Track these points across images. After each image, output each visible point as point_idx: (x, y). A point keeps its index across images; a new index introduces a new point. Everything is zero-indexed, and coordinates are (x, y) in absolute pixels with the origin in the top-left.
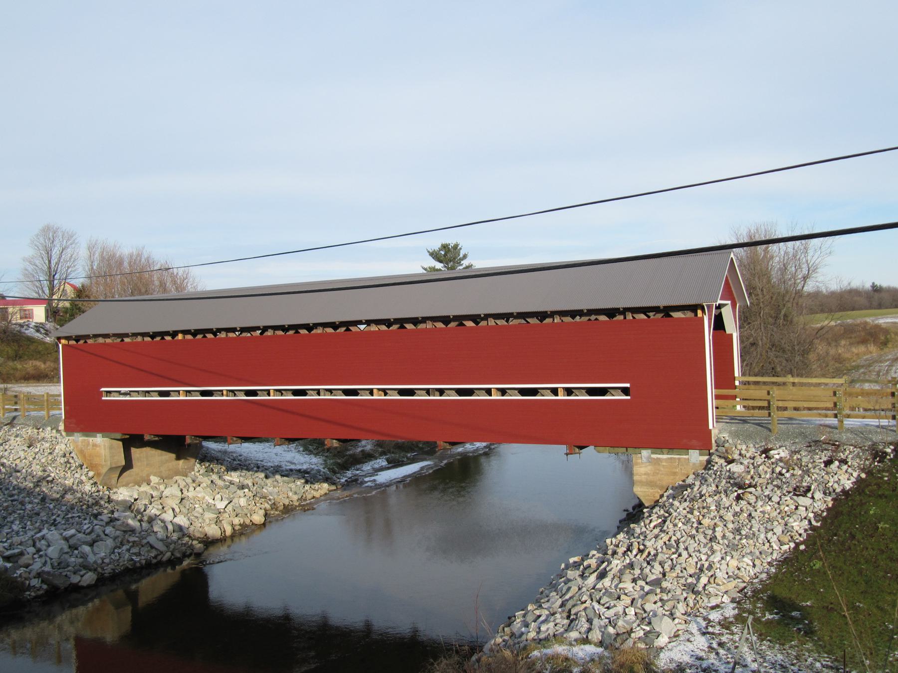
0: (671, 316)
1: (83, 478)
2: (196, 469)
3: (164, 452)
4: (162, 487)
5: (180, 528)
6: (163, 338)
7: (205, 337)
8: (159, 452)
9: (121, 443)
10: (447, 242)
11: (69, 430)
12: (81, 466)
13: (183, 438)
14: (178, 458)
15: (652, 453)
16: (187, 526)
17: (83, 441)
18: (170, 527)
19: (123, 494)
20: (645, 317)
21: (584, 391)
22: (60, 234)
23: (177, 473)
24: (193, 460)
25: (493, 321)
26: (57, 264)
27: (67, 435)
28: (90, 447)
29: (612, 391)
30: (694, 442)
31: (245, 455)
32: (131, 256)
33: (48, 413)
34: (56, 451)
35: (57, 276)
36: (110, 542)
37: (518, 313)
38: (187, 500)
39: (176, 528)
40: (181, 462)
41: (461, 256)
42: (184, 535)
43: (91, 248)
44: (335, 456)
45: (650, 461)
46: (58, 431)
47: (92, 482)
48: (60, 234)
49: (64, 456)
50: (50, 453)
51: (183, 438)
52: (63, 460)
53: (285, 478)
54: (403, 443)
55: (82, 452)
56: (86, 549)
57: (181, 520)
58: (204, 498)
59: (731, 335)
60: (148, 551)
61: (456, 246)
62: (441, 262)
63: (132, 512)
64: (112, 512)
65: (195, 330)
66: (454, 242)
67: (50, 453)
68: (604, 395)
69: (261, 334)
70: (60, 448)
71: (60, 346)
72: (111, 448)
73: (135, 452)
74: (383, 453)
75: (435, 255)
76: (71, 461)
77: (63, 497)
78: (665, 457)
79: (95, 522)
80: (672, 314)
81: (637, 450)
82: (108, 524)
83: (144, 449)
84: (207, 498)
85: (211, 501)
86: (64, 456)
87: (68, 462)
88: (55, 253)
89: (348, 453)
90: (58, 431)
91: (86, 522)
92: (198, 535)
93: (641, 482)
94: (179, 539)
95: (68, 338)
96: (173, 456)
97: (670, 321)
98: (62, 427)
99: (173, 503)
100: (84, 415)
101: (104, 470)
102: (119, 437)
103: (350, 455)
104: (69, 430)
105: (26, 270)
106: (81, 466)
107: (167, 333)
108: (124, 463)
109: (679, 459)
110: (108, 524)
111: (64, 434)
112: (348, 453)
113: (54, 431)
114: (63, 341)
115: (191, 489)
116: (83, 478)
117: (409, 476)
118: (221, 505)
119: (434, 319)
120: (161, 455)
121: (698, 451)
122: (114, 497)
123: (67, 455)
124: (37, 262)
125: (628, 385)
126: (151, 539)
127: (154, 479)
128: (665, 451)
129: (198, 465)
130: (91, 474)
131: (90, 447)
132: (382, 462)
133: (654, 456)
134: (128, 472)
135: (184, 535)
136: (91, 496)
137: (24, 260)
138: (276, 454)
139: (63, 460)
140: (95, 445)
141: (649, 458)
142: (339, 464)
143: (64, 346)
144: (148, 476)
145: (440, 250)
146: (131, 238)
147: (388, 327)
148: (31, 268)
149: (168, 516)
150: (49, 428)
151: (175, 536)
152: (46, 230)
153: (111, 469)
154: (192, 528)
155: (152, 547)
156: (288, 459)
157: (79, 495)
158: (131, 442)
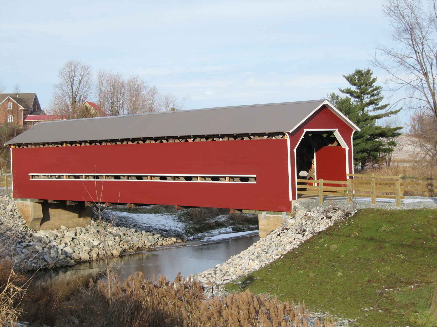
0: (188, 141)
1: (20, 224)
2: (91, 224)
3: (70, 213)
4: (65, 232)
5: (66, 253)
6: (243, 139)
7: (213, 140)
8: (67, 212)
9: (40, 205)
10: (360, 69)
11: (15, 197)
12: (20, 217)
13: (65, 202)
14: (80, 217)
15: (267, 213)
16: (71, 252)
17: (21, 203)
18: (60, 252)
19: (41, 234)
20: (179, 142)
21: (239, 179)
22: (79, 67)
23: (79, 225)
24: (89, 219)
25: (149, 141)
26: (78, 89)
27: (15, 200)
28: (24, 207)
29: (250, 179)
30: (284, 208)
31: (136, 219)
32: (129, 82)
33: (7, 188)
34: (7, 208)
35: (77, 98)
36: (22, 256)
37: (110, 140)
38: (75, 238)
39: (63, 253)
40: (81, 219)
41: (371, 80)
42: (67, 257)
43: (100, 78)
44: (195, 223)
45: (266, 217)
46: (10, 197)
47: (24, 226)
48: (79, 67)
49: (12, 211)
50: (4, 209)
51: (65, 202)
52: (10, 213)
53: (148, 233)
54: (252, 218)
55: (21, 209)
56: (8, 258)
57: (68, 249)
58: (88, 239)
59: (345, 149)
60: (42, 263)
61: (368, 73)
62: (355, 85)
63: (41, 243)
64: (30, 242)
65: (207, 135)
66: (366, 69)
67: (4, 209)
68: (247, 181)
69: (193, 140)
70: (10, 207)
71: (11, 149)
72: (34, 207)
73: (52, 212)
74: (231, 225)
75: (351, 80)
76: (15, 214)
77: (5, 232)
78: (272, 216)
79: (18, 246)
80: (188, 140)
81: (260, 212)
82: (25, 247)
83: (58, 210)
84: (89, 239)
85: (91, 241)
86: (12, 211)
87: (13, 215)
88: (76, 83)
89: (205, 222)
90: (10, 197)
91: (14, 245)
92: (76, 257)
93: (262, 229)
94: (64, 258)
95: (14, 145)
96: (77, 215)
97: (272, 140)
98: (12, 195)
99: (67, 240)
100: (23, 189)
101: (31, 220)
102: (37, 201)
103: (206, 223)
104: (15, 197)
105: (57, 94)
106: (20, 217)
107: (163, 138)
108: (42, 216)
109: (278, 217)
110: (25, 247)
111: (13, 199)
112: (205, 222)
113: (8, 197)
114: (12, 147)
115: (83, 234)
116: (20, 224)
117: (234, 237)
118: (95, 243)
119: (229, 136)
120: (69, 214)
121: (285, 213)
122: (35, 234)
123: (13, 211)
124: (64, 88)
125: (255, 176)
126: (46, 257)
127: (63, 227)
128: (272, 212)
129: (93, 222)
130: (24, 222)
131: (24, 207)
132: (229, 229)
133: (267, 215)
134: (47, 222)
135: (67, 257)
136: (21, 233)
137: (55, 86)
138: (157, 221)
139: (10, 213)
140: (27, 206)
141: (265, 216)
142: (196, 228)
143: (13, 149)
144: (60, 225)
145: (354, 75)
146: (126, 71)
147: (133, 142)
148: (59, 92)
149: (61, 247)
150: (6, 196)
151: (62, 257)
152: (70, 64)
153: (35, 219)
154: (73, 255)
155: (45, 261)
156: (163, 223)
157: (14, 232)
158: (46, 206)
